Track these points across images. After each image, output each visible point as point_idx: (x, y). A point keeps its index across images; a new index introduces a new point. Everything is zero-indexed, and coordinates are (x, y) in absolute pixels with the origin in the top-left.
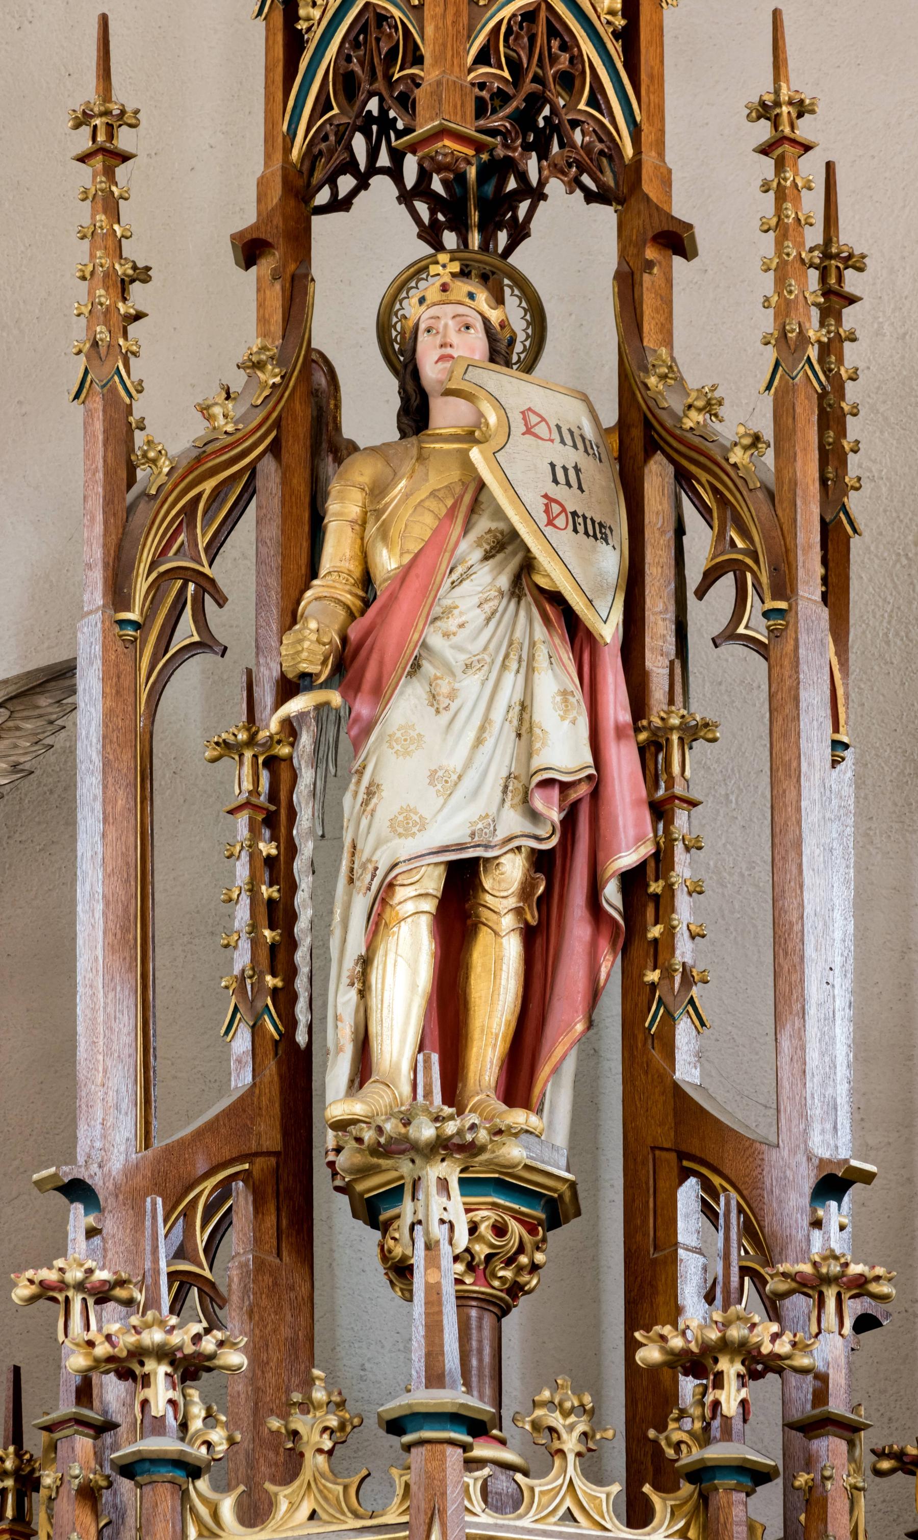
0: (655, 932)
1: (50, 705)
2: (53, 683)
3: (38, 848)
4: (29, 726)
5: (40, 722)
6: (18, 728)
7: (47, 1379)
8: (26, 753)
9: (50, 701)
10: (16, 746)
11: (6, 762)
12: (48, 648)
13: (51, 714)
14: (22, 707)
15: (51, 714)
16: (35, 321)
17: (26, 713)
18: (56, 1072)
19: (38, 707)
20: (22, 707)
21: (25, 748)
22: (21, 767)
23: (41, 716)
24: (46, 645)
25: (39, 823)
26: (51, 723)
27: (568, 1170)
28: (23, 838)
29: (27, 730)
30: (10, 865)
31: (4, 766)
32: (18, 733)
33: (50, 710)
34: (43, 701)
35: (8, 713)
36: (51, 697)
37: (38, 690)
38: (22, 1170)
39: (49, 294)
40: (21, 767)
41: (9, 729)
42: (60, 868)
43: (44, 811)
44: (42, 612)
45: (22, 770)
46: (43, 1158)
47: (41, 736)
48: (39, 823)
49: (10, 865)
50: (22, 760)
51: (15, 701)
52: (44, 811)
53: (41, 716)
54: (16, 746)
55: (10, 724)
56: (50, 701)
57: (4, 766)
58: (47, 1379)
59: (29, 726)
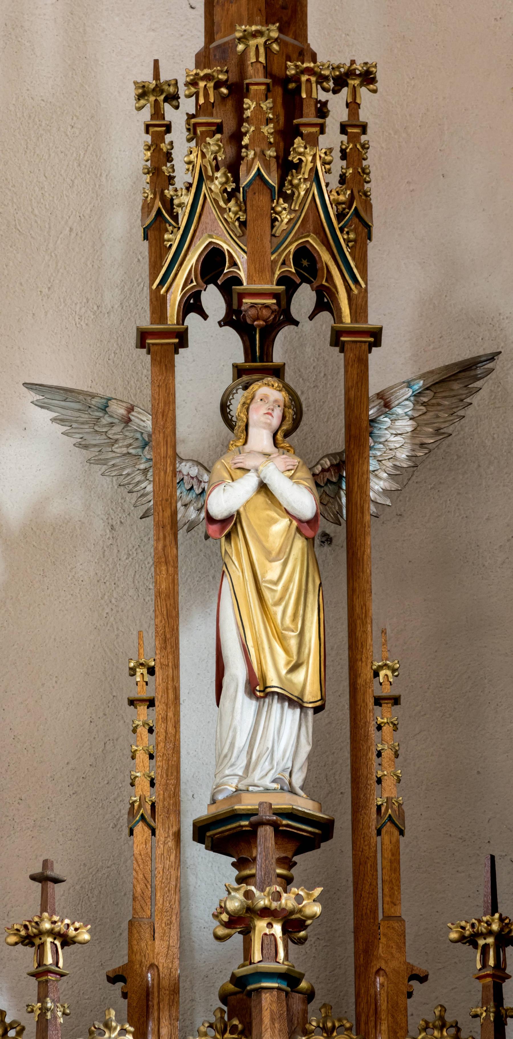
0: (368, 587)
1: (461, 388)
2: (463, 374)
3: (430, 487)
4: (446, 403)
5: (454, 400)
6: (439, 404)
7: (445, 864)
8: (445, 422)
9: (461, 386)
10: (438, 417)
11: (432, 428)
12: (434, 349)
13: (462, 394)
14: (442, 390)
15: (462, 394)
16: (418, 128)
17: (444, 394)
18: (447, 644)
19: (453, 390)
20: (442, 390)
21: (444, 418)
22: (442, 431)
23: (455, 396)
24: (432, 347)
25: (430, 469)
26: (462, 400)
27: (321, 811)
28: (419, 480)
29: (444, 405)
30: (410, 499)
31: (431, 430)
32: (439, 408)
33: (461, 392)
34: (456, 386)
35: (432, 394)
36: (461, 383)
37: (453, 378)
38: (422, 713)
39: (428, 110)
40: (442, 431)
41: (433, 405)
42: (446, 501)
43: (433, 461)
44: (428, 324)
45: (444, 433)
46: (438, 705)
47: (455, 410)
48: (430, 469)
49: (410, 499)
50: (443, 426)
51: (437, 386)
52: (433, 461)
53: (455, 396)
54: (438, 417)
55: (434, 401)
56: (461, 386)
57: (431, 430)
58: (445, 864)
59: (446, 403)
